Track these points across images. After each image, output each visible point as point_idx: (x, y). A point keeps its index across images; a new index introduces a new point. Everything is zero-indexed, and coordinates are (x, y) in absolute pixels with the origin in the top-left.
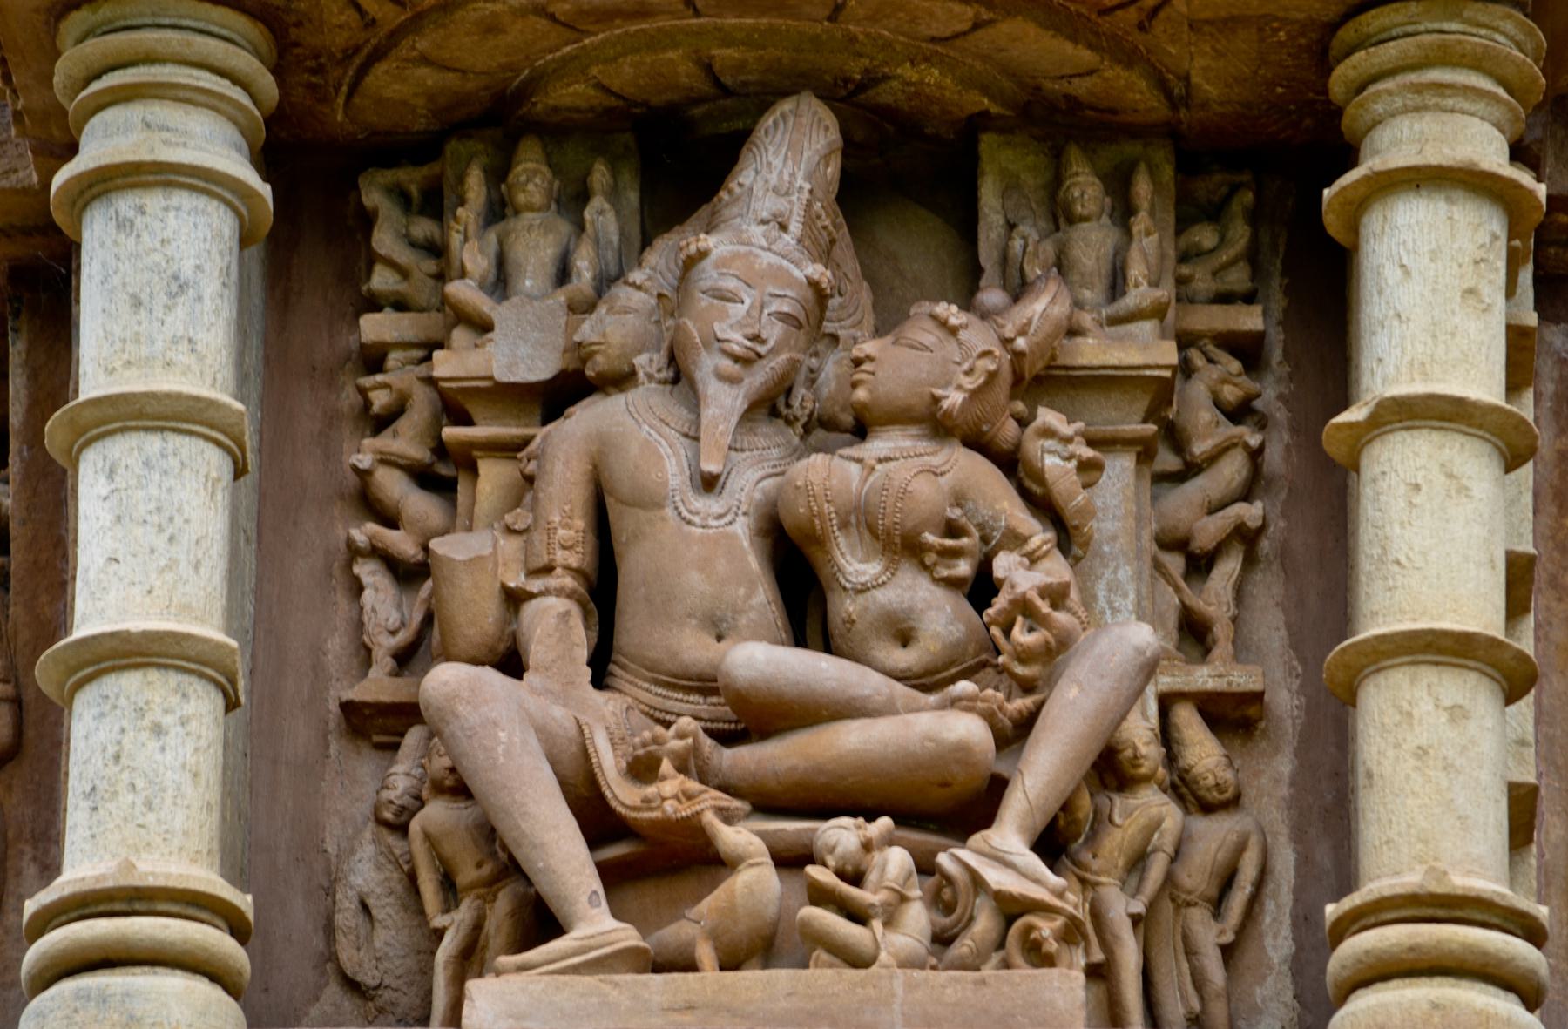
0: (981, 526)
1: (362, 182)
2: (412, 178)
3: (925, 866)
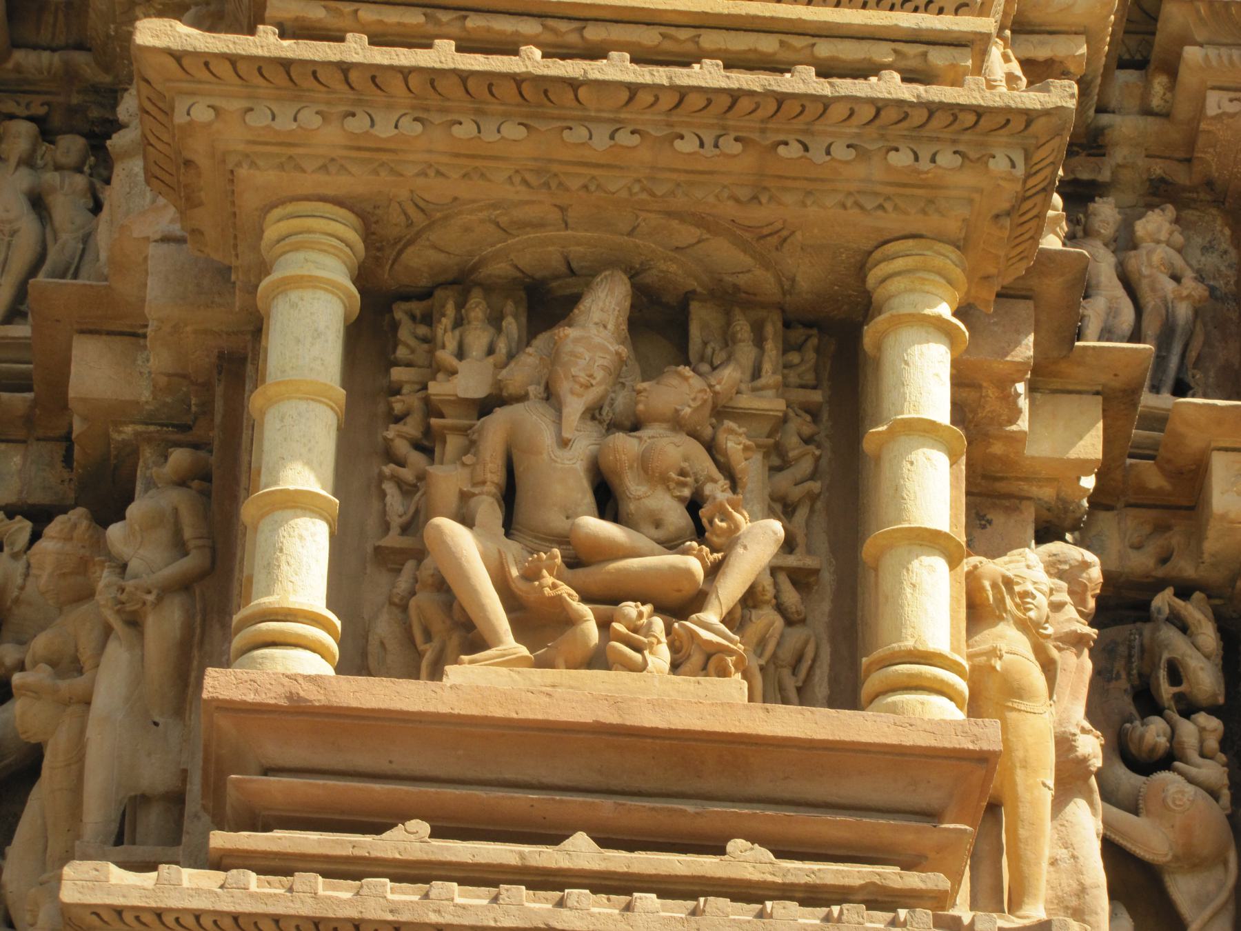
0: (695, 474)
1: (395, 307)
2: (417, 307)
3: (669, 631)
